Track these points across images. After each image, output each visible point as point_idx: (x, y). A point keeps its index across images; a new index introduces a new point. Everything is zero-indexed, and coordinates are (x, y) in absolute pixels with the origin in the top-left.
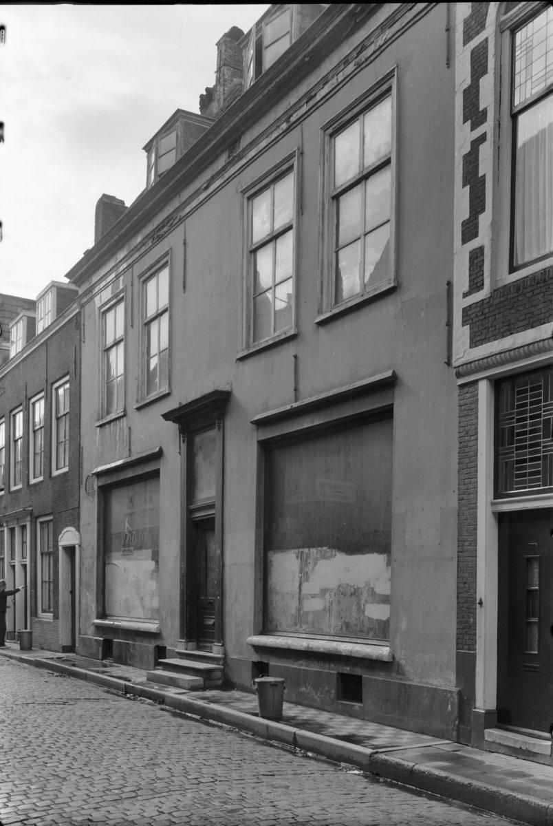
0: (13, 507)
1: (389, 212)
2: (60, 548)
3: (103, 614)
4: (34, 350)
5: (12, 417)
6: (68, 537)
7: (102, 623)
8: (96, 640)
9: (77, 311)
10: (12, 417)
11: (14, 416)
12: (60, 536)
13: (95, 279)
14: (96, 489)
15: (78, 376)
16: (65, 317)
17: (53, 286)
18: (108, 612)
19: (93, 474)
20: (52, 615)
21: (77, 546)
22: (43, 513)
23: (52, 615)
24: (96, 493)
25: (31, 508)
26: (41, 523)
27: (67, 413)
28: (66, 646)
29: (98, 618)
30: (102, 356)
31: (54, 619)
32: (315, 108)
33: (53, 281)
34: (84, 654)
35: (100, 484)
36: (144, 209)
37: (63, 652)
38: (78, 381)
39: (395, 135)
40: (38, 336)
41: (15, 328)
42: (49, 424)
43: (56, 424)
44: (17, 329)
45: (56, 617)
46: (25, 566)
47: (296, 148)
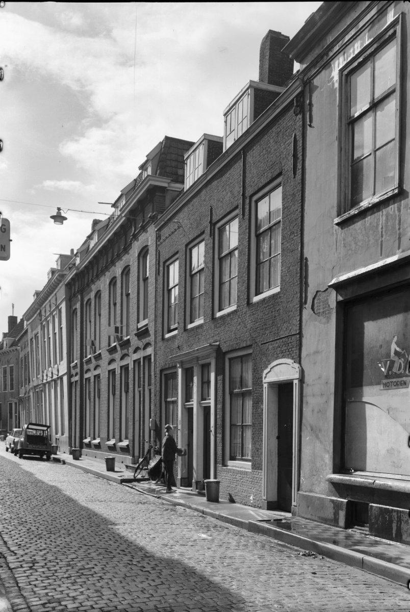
0: (190, 346)
1: (394, 134)
2: (265, 385)
3: (341, 466)
4: (184, 204)
5: (166, 267)
6: (282, 370)
7: (342, 480)
8: (332, 501)
9: (300, 90)
10: (166, 267)
11: (191, 250)
12: (266, 371)
13: (330, 39)
14: (333, 305)
15: (299, 172)
16: (278, 107)
17: (250, 87)
18: (225, 464)
19: (330, 286)
20: (250, 463)
21: (296, 382)
22: (235, 346)
23: (250, 463)
24: (335, 311)
25: (217, 343)
26: (230, 359)
27: (203, 269)
28: (271, 502)
29: (334, 472)
30: (346, 129)
31: (252, 468)
32: (360, 32)
33: (205, 135)
34: (309, 516)
35: (340, 298)
36: (299, 46)
37: (268, 509)
38: (299, 176)
39: (399, 74)
40: (187, 191)
41: (192, 157)
42: (246, 244)
43: (218, 265)
44: (195, 159)
45: (256, 466)
46: (207, 410)
47: (400, 13)
